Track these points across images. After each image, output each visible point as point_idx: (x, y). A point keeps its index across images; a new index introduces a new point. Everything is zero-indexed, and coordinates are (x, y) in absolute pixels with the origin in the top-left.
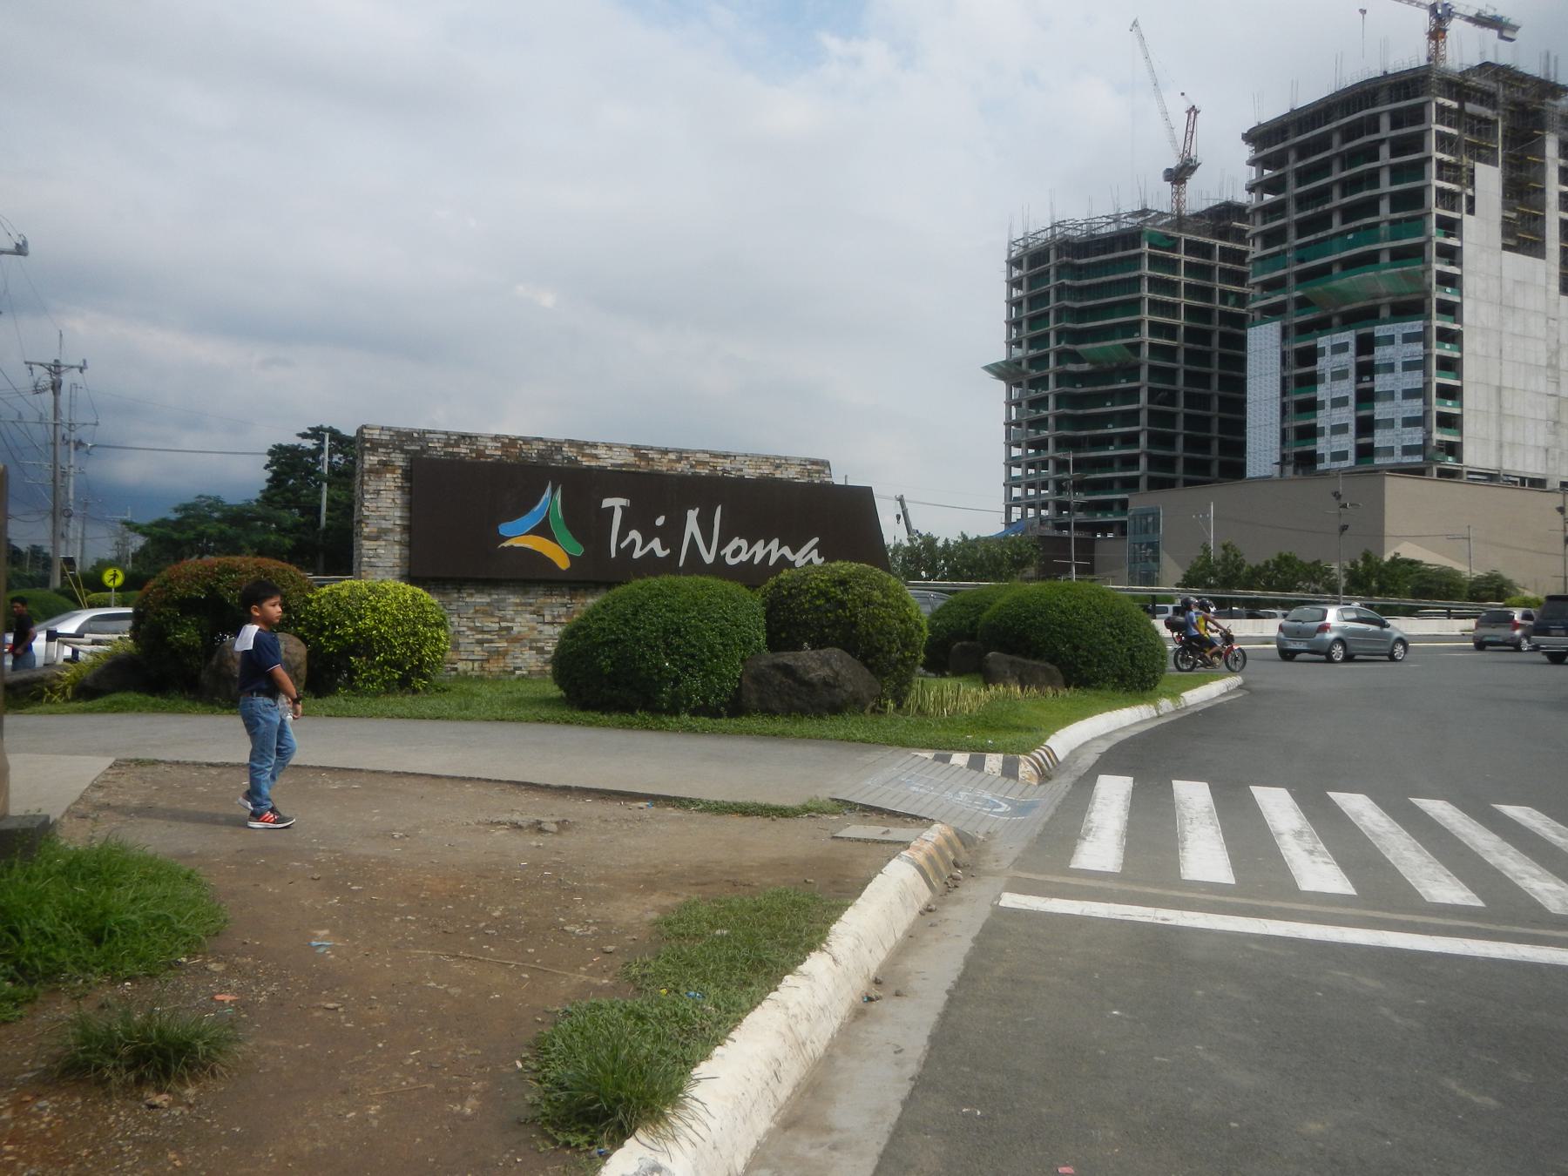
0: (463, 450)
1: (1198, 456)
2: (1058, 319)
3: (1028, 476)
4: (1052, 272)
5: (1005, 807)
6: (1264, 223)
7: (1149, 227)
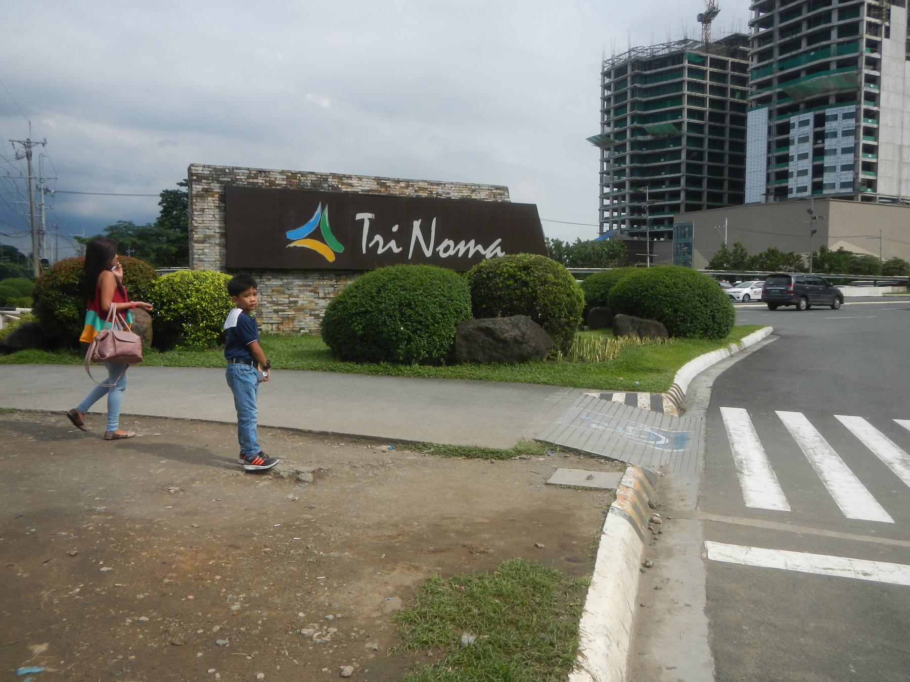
0: (260, 180)
1: (716, 191)
2: (632, 109)
3: (613, 204)
4: (629, 79)
5: (664, 440)
6: (759, 46)
7: (688, 50)
